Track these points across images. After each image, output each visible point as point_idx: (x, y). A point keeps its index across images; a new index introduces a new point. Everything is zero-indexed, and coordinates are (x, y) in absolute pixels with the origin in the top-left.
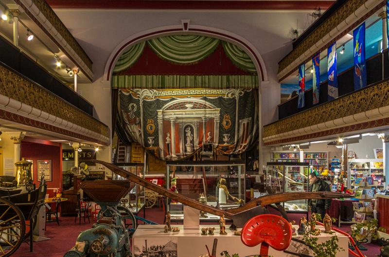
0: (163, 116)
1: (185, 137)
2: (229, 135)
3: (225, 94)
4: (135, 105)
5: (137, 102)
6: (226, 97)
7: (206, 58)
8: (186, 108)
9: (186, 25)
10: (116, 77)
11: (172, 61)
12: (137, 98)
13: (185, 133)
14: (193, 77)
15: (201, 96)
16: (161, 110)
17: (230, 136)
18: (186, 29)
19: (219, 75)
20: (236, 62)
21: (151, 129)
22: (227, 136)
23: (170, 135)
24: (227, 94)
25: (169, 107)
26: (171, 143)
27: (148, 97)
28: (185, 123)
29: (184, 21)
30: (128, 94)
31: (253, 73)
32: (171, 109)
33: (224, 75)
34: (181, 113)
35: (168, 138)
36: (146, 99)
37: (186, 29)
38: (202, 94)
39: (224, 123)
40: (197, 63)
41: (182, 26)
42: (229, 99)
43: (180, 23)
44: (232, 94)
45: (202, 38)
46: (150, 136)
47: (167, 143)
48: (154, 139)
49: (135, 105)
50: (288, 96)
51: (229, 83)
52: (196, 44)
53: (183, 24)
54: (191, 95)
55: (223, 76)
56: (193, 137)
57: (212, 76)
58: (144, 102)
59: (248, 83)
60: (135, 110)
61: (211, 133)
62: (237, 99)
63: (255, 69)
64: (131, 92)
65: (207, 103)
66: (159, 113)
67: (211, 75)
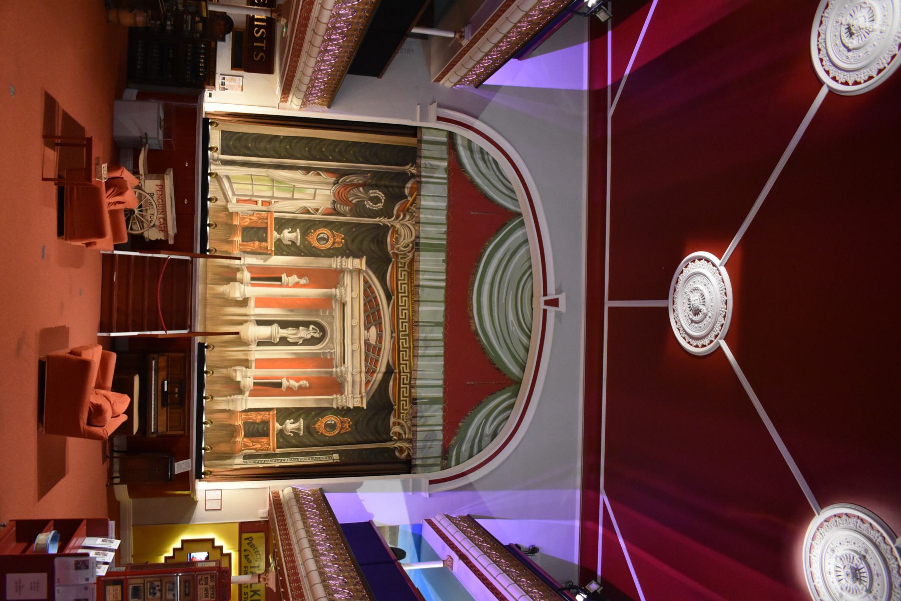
0: (351, 272)
1: (296, 325)
2: (301, 434)
3: (399, 417)
4: (380, 205)
5: (387, 212)
6: (392, 420)
7: (483, 350)
8: (367, 328)
9: (554, 303)
10: (445, 139)
11: (477, 271)
12: (395, 212)
13: (306, 324)
14: (441, 319)
15: (395, 401)
16: (364, 267)
17: (298, 434)
18: (547, 303)
19: (445, 381)
20: (475, 417)
21: (319, 240)
22: (299, 429)
23: (304, 286)
24: (399, 424)
25: (370, 287)
26: (281, 286)
27: (397, 239)
28: (331, 324)
29: (562, 298)
30: (407, 191)
31: (446, 459)
32: (365, 290)
33: (444, 393)
34: (356, 314)
35: (294, 279)
36: (393, 233)
37: (547, 303)
38: (399, 364)
39: (331, 419)
40: (473, 328)
41: (552, 295)
42: (388, 429)
43: (559, 291)
44: (400, 434)
45: (524, 340)
46: (304, 234)
47: (284, 276)
48: (293, 243)
49: (380, 205)
50: (394, 541)
51: (425, 403)
52: (514, 328)
53: (556, 297)
54: (399, 339)
55: (441, 390)
56: (295, 344)
57: (443, 309)
58: (386, 228)
59: (424, 448)
60: (369, 205)
61: (305, 388)
62: (389, 445)
63: (457, 463)
64: (410, 199)
65: (380, 376)
66: (357, 261)
67: (445, 361)
